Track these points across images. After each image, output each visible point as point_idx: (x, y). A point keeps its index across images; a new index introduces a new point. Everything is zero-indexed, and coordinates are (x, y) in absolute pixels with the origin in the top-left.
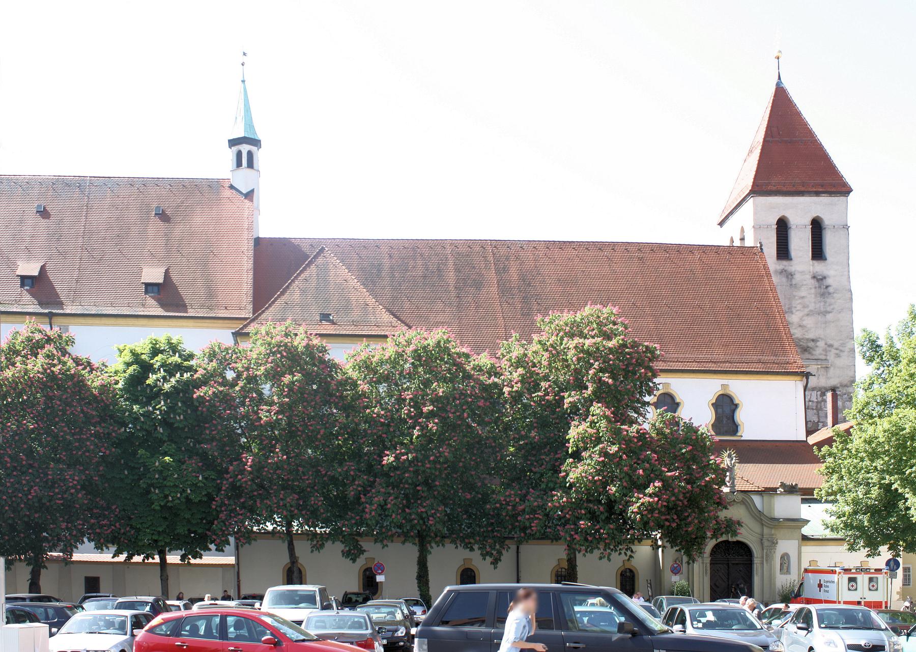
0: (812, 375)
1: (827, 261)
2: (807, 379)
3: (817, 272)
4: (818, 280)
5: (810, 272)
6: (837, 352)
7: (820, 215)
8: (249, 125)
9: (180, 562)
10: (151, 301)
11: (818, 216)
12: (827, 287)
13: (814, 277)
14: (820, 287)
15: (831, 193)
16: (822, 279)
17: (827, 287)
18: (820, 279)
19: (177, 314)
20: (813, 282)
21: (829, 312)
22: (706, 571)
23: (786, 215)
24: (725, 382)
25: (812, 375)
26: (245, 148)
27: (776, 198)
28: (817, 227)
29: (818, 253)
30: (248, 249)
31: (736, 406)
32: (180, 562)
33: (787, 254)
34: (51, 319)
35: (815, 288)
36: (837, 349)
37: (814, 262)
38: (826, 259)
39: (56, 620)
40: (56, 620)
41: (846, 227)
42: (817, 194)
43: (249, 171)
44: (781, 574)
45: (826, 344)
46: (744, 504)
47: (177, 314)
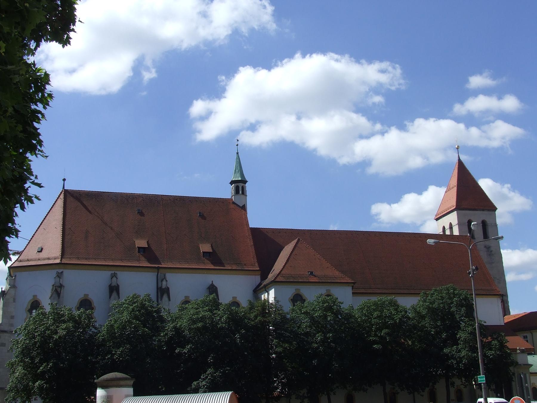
7: (485, 219)
8: (242, 175)
10: (206, 261)
11: (484, 220)
12: (491, 251)
13: (485, 247)
15: (489, 210)
16: (489, 248)
17: (491, 251)
18: (488, 248)
19: (219, 268)
23: (486, 220)
26: (241, 185)
27: (471, 211)
28: (484, 224)
29: (486, 236)
30: (248, 234)
34: (158, 270)
35: (486, 252)
36: (498, 279)
39: (7, 198)
40: (7, 198)
42: (483, 210)
43: (242, 196)
47: (219, 268)
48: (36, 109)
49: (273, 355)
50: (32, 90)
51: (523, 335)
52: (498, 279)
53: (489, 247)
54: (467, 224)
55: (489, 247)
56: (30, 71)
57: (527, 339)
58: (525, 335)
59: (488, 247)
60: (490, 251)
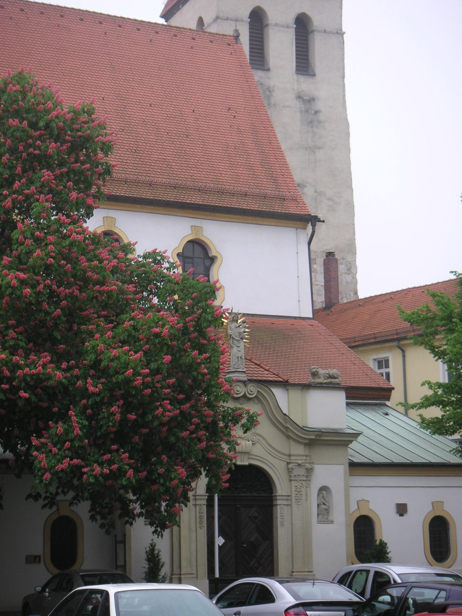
0: (320, 221)
1: (317, 77)
2: (314, 226)
3: (302, 91)
4: (304, 101)
5: (294, 90)
6: (331, 203)
9: (162, 21)
12: (316, 112)
13: (299, 97)
14: (307, 111)
17: (316, 112)
20: (297, 104)
21: (320, 148)
22: (278, 478)
24: (197, 222)
25: (320, 221)
26: (195, 576)
31: (213, 260)
32: (162, 21)
33: (263, 61)
36: (329, 199)
37: (300, 76)
38: (314, 75)
41: (340, 34)
44: (319, 522)
45: (316, 192)
46: (259, 400)
48: (28, 125)
49: (88, 409)
50: (88, 401)
51: (375, 357)
52: (329, 199)
53: (312, 100)
54: (249, 20)
55: (312, 100)
56: (73, 307)
57: (387, 370)
58: (382, 355)
59: (308, 98)
60: (313, 112)
